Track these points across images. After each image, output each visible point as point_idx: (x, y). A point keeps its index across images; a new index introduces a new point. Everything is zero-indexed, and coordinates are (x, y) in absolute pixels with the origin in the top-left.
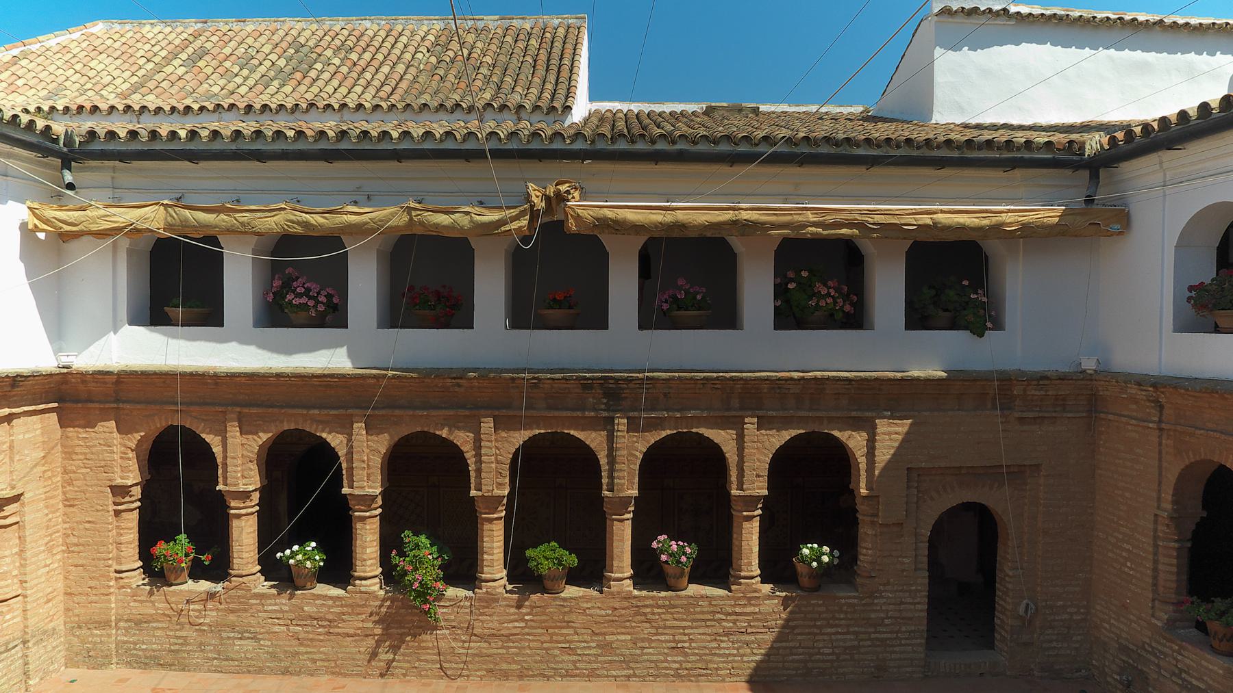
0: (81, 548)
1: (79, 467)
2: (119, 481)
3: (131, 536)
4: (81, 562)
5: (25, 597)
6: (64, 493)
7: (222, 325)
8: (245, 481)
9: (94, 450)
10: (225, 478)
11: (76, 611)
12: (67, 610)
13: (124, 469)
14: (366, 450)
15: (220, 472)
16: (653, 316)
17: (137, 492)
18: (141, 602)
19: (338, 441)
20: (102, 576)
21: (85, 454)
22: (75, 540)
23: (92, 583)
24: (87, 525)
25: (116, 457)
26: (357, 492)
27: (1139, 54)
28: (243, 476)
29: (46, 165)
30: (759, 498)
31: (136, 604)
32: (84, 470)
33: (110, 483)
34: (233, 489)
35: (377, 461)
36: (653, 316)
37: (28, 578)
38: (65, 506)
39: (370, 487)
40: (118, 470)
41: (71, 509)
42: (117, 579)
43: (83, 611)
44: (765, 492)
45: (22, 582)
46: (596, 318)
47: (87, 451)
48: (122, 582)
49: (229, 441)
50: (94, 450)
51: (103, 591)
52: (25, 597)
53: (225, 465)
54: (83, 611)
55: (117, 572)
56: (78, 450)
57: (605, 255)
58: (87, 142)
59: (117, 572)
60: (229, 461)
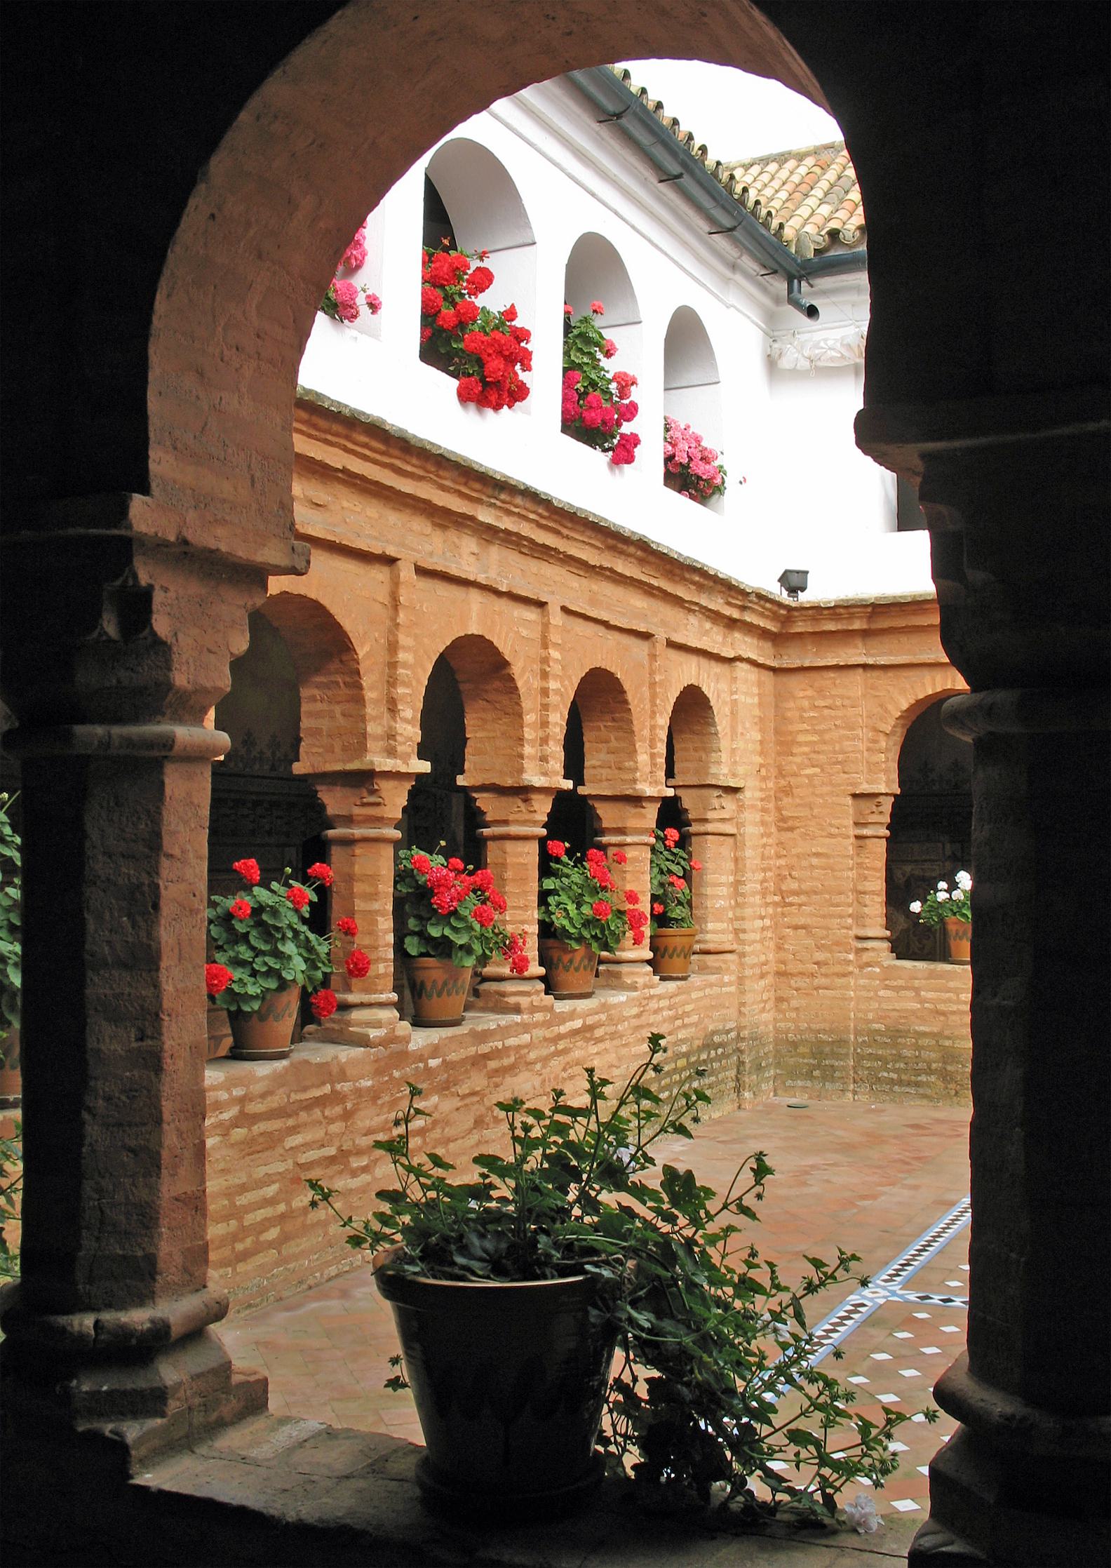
0: (803, 898)
1: (801, 766)
2: (865, 788)
3: (878, 884)
4: (802, 921)
5: (742, 955)
6: (779, 809)
9: (827, 737)
11: (794, 1003)
12: (779, 1000)
17: (887, 804)
18: (897, 989)
20: (838, 944)
22: (794, 886)
23: (820, 956)
24: (815, 861)
25: (862, 746)
27: (772, 32)
29: (765, 290)
31: (888, 993)
32: (809, 771)
37: (747, 925)
38: (780, 829)
41: (789, 834)
42: (859, 951)
43: (803, 1002)
45: (737, 932)
48: (866, 957)
50: (827, 737)
51: (838, 969)
52: (742, 955)
54: (803, 1002)
55: (859, 938)
56: (801, 738)
59: (859, 938)
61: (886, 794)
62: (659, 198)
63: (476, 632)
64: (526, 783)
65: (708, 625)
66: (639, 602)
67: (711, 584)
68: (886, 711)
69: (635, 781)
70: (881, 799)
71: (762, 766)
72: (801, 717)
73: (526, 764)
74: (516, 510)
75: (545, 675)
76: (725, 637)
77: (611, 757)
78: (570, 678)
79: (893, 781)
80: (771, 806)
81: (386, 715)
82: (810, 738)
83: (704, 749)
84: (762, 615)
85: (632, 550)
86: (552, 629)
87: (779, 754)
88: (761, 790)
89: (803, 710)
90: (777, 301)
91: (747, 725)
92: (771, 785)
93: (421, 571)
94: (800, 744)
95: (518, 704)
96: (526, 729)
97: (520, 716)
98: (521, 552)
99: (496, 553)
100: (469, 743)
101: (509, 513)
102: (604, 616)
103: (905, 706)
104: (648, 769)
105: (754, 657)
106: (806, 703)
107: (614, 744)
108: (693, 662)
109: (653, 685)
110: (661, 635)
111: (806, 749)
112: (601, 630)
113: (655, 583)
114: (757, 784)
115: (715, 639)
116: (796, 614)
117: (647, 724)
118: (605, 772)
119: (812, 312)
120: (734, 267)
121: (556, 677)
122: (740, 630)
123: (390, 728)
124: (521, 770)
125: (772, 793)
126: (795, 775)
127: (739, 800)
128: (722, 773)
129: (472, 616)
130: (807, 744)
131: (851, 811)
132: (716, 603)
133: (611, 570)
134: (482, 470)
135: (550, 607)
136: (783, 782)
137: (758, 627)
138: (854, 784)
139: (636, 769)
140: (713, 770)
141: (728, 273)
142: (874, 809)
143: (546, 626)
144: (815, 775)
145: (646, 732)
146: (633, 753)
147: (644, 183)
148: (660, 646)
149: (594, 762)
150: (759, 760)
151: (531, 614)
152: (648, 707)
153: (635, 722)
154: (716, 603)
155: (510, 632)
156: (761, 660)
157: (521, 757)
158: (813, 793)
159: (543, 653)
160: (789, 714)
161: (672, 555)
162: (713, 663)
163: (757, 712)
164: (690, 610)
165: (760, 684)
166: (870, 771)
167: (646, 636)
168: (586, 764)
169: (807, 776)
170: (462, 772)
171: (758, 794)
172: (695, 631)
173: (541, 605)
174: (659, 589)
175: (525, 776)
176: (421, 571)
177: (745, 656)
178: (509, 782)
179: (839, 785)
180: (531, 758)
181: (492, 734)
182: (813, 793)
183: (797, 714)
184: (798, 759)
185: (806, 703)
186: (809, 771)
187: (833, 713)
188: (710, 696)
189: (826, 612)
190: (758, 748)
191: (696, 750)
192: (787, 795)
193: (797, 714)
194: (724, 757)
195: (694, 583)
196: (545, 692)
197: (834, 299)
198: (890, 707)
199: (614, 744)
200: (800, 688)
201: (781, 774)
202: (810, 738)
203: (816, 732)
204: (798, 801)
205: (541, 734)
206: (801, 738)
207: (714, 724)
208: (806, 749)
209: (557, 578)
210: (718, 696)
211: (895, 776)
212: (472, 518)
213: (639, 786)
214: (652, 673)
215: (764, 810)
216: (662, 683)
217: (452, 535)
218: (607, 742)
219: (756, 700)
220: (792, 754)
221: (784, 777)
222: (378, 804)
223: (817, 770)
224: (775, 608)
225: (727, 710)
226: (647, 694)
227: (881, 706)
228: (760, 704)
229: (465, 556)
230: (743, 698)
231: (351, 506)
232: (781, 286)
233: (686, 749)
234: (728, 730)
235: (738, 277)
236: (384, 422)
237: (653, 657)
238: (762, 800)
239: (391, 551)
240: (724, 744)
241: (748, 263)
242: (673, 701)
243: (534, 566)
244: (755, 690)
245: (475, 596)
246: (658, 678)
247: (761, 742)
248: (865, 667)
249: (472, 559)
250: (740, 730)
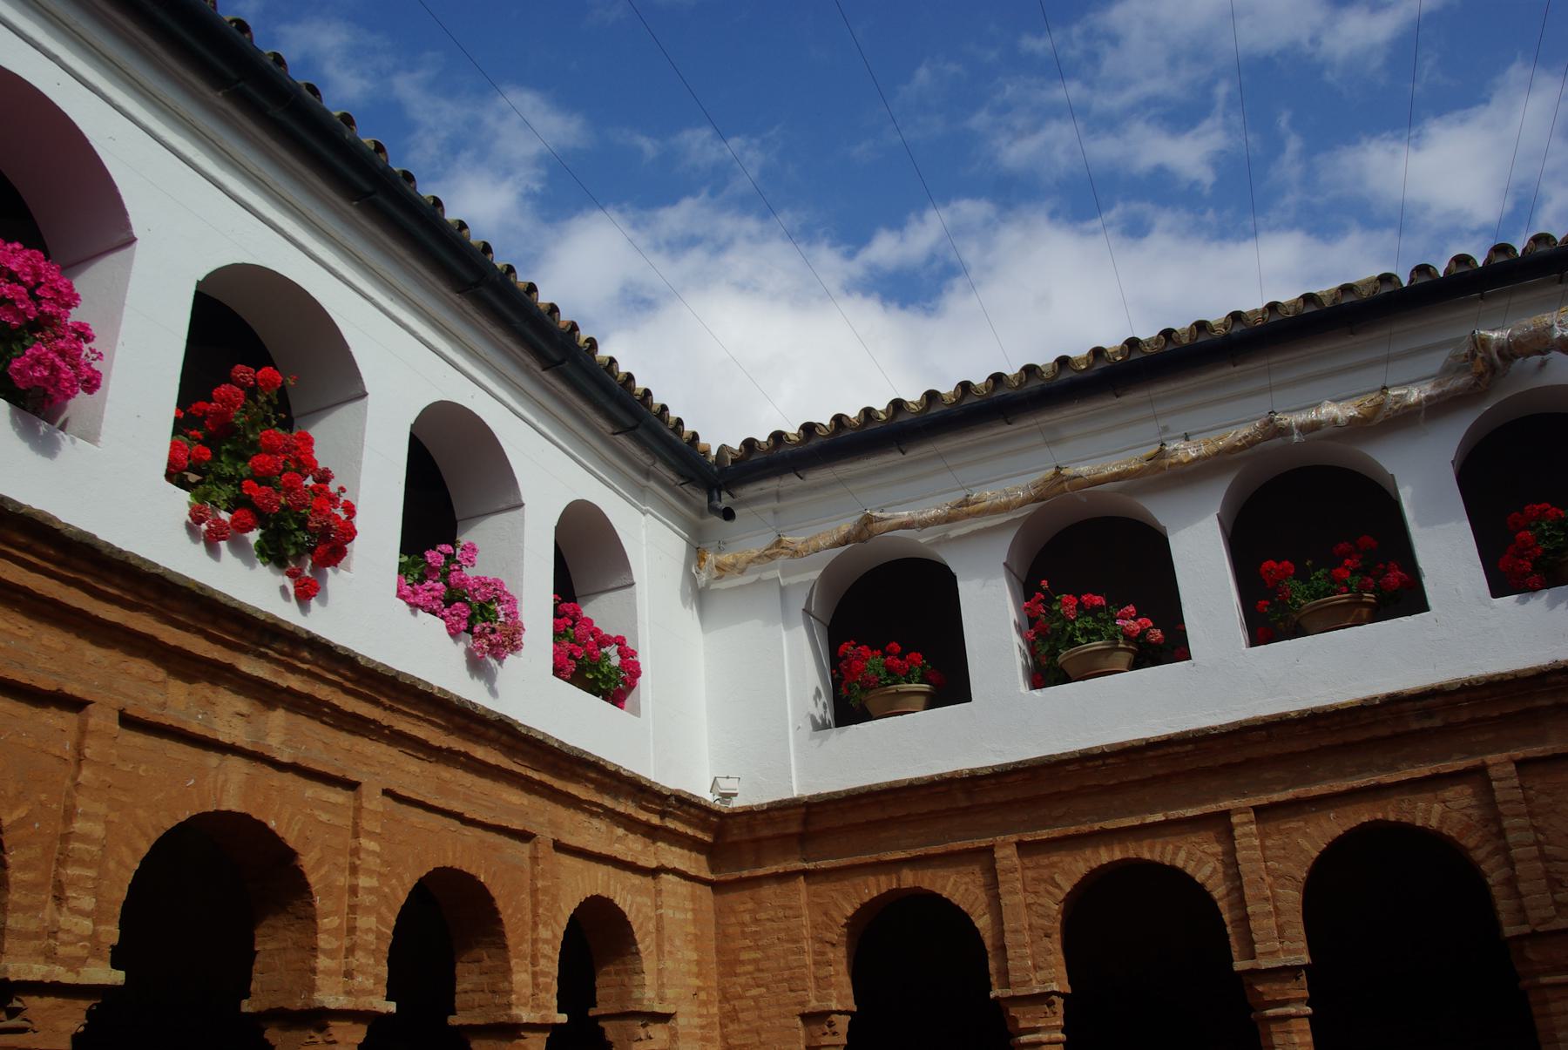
1: (747, 987)
2: (814, 1005)
7: (967, 697)
8: (1040, 975)
9: (771, 952)
10: (1004, 973)
13: (822, 983)
14: (1269, 880)
15: (992, 966)
16: (1268, 620)
17: (842, 1023)
19: (1207, 870)
21: (755, 961)
25: (809, 960)
26: (1264, 964)
28: (1036, 967)
30: (1299, 968)
32: (754, 992)
33: (799, 1009)
34: (1022, 991)
35: (1292, 897)
36: (1268, 620)
39: (1289, 952)
40: (811, 983)
44: (1306, 959)
46: (1401, 594)
47: (758, 955)
49: (1005, 901)
53: (1002, 949)
56: (744, 956)
57: (953, 579)
58: (994, 390)
60: (1009, 939)
61: (839, 1012)
62: (546, 388)
63: (234, 808)
64: (317, 1005)
65: (620, 831)
66: (515, 797)
67: (615, 783)
68: (832, 919)
69: (509, 1005)
70: (834, 1017)
71: (699, 988)
72: (743, 932)
73: (319, 980)
74: (305, 666)
75: (354, 870)
76: (646, 846)
77: (485, 979)
78: (400, 877)
79: (846, 997)
80: (716, 1033)
81: (51, 905)
82: (753, 955)
83: (626, 971)
84: (684, 822)
85: (492, 733)
86: (364, 814)
87: (721, 975)
88: (700, 1016)
89: (743, 924)
90: (701, 514)
91: (677, 942)
92: (714, 1010)
93: (129, 722)
94: (742, 963)
95: (311, 905)
96: (321, 936)
97: (312, 919)
98: (323, 722)
99: (279, 718)
100: (258, 958)
101: (293, 670)
102: (457, 807)
103: (850, 911)
104: (528, 991)
105: (682, 867)
106: (747, 918)
107: (487, 963)
108: (602, 871)
109: (534, 892)
110: (546, 835)
111: (750, 968)
112: (455, 824)
113: (536, 776)
114: (695, 1009)
115: (632, 847)
116: (730, 821)
117: (529, 937)
118: (477, 997)
119: (728, 515)
120: (647, 474)
121: (370, 873)
122: (663, 840)
123: (54, 922)
124: (312, 988)
125: (716, 1019)
126: (740, 997)
127: (671, 1028)
128: (648, 997)
129: (230, 788)
130: (751, 962)
131: (802, 1033)
132: (626, 807)
133: (466, 755)
134: (234, 605)
135: (364, 789)
136: (727, 1007)
137: (685, 835)
138: (803, 1003)
139: (510, 992)
140: (636, 994)
141: (643, 481)
142: (827, 1029)
143: (358, 810)
144: (761, 996)
145: (526, 947)
146: (507, 972)
147: (526, 370)
148: (545, 849)
149: (467, 986)
150: (697, 982)
151: (337, 796)
152: (528, 917)
153: (509, 935)
154: (626, 807)
155: (295, 813)
156: (693, 872)
157: (314, 971)
158: (760, 1017)
159: (352, 843)
160: (731, 930)
161: (550, 742)
162: (629, 874)
163: (691, 929)
164: (592, 814)
165: (694, 898)
166: (818, 987)
167: (524, 836)
168: (458, 988)
169: (753, 998)
170: (247, 995)
171: (696, 1021)
172: (593, 834)
173: (352, 786)
174: (541, 783)
175: (317, 996)
176: (129, 722)
177: (671, 866)
178: (298, 1004)
179: (786, 1005)
180: (329, 973)
181: (283, 945)
182: (760, 1017)
183: (738, 929)
184: (742, 980)
185: (747, 918)
186: (754, 992)
187: (775, 925)
188: (626, 910)
189: (760, 817)
190: (695, 969)
191: (617, 973)
192: (732, 1021)
193: (738, 929)
194: (649, 979)
195: (592, 781)
196: (354, 890)
197: (755, 508)
198: (835, 914)
199: (487, 963)
200: (741, 902)
201: (725, 997)
202: (753, 955)
203: (758, 948)
204: (744, 1027)
205: (346, 942)
206: (744, 956)
207: (634, 943)
208: (750, 968)
209: (384, 758)
210: (639, 911)
211: (849, 991)
212: (231, 668)
213: (515, 1011)
214: (534, 878)
215: (705, 1039)
216: (546, 891)
217: (203, 689)
218: (479, 961)
219: (690, 916)
220: (736, 975)
221: (728, 1001)
222: (23, 1030)
223: (763, 990)
224: (703, 815)
225: (651, 926)
226: (528, 903)
227: (826, 914)
228: (695, 921)
229: (228, 716)
230: (670, 912)
231: (13, 629)
232: (702, 498)
233: (608, 973)
234: (653, 948)
235: (652, 484)
236: (94, 537)
237: (534, 859)
238: (702, 1027)
239: (74, 689)
240: (649, 964)
241: (660, 469)
242: (568, 913)
243: (344, 740)
244: (689, 905)
245: (236, 764)
246: (540, 884)
247: (698, 963)
248: (806, 873)
249: (237, 721)
250: (667, 947)
